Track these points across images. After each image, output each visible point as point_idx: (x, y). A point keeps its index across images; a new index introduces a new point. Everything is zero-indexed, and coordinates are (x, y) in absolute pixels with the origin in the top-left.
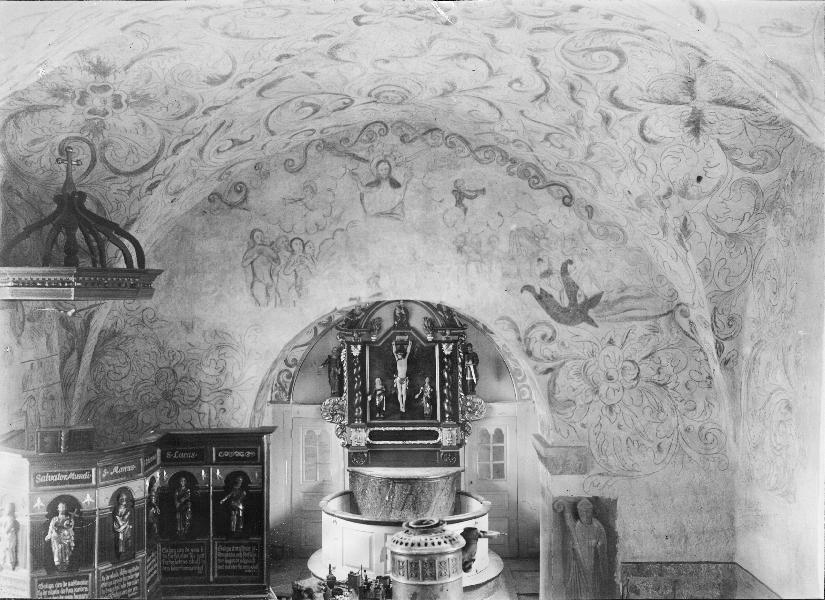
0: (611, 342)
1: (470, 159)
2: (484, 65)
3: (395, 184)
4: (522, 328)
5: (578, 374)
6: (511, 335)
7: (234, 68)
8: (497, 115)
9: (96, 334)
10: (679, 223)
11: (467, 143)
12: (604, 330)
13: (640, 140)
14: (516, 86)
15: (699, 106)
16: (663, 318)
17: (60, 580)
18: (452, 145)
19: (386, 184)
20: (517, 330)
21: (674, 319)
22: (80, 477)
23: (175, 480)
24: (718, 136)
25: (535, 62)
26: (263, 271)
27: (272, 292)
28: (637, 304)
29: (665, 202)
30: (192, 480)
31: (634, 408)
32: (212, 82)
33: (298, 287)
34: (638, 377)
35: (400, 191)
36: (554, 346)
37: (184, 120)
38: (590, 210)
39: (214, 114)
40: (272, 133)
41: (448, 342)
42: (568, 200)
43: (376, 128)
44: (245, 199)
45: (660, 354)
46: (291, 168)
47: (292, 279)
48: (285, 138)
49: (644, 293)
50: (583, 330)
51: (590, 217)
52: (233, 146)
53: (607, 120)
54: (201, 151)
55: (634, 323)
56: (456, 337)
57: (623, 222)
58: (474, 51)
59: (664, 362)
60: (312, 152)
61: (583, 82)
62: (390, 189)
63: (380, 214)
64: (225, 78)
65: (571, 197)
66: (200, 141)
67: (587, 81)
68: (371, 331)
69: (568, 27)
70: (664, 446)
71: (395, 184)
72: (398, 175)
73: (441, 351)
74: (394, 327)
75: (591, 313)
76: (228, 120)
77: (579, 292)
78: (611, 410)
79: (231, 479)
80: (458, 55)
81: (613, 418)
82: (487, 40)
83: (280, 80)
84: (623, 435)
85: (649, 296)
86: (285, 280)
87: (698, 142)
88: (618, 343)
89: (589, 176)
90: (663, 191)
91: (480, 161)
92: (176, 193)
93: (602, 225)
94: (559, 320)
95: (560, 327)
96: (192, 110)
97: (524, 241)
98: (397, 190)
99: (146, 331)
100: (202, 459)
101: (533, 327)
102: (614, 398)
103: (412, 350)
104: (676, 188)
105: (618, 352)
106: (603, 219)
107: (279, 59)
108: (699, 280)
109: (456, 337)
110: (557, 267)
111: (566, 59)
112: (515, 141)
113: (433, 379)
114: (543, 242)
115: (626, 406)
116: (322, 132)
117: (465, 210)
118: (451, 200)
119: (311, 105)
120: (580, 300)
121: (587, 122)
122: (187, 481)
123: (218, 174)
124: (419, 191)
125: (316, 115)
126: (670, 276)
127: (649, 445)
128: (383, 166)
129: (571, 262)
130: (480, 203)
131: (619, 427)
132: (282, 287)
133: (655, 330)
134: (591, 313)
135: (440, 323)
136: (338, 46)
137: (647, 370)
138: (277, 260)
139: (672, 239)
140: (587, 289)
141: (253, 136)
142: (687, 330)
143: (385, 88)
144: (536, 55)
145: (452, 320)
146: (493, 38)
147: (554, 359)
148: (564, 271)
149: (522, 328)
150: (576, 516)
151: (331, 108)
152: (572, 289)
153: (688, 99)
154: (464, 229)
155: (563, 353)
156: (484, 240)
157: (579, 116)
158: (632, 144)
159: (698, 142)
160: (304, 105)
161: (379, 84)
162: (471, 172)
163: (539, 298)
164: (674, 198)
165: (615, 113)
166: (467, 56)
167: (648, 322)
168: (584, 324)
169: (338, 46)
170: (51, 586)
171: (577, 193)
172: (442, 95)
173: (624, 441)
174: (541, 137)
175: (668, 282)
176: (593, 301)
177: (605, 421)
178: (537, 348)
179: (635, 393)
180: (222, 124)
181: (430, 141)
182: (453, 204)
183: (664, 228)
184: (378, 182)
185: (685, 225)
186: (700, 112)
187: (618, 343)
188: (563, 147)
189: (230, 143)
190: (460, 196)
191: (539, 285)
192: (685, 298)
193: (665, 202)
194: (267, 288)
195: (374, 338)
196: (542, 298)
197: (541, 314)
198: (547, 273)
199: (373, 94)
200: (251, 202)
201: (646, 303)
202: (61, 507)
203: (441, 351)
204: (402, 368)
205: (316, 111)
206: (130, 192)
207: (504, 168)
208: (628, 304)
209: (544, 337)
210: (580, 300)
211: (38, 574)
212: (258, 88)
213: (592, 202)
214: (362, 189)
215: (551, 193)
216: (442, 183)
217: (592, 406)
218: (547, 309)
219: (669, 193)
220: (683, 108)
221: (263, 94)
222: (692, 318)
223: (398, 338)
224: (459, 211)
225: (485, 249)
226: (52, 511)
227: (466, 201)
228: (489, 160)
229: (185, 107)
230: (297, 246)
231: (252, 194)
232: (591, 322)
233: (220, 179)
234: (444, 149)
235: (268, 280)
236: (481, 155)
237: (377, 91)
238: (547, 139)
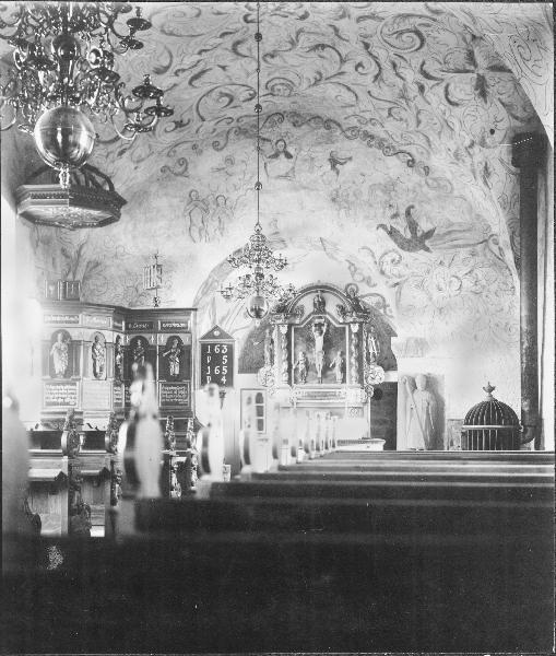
1: (342, 137)
3: (289, 156)
4: (378, 255)
6: (369, 260)
7: (171, 61)
8: (354, 99)
9: (85, 264)
10: (482, 167)
11: (339, 125)
12: (434, 255)
13: (446, 103)
15: (481, 72)
16: (480, 246)
17: (59, 384)
18: (328, 128)
19: (282, 156)
20: (373, 256)
21: (487, 246)
22: (72, 319)
23: (134, 342)
24: (498, 96)
25: (367, 46)
26: (197, 218)
27: (203, 233)
28: (459, 235)
29: (470, 150)
30: (145, 341)
33: (222, 229)
36: (400, 267)
38: (427, 170)
41: (354, 323)
42: (411, 163)
43: (276, 118)
44: (186, 169)
45: (475, 271)
46: (216, 146)
47: (217, 223)
49: (465, 228)
50: (421, 255)
51: (427, 173)
52: (176, 127)
53: (422, 89)
55: (458, 249)
56: (362, 320)
57: (449, 176)
58: (327, 42)
59: (480, 276)
60: (232, 136)
61: (402, 61)
62: (286, 160)
63: (279, 177)
64: (167, 68)
65: (413, 161)
67: (402, 57)
68: (295, 315)
69: (381, 15)
70: (361, 179)
71: (289, 156)
72: (291, 150)
73: (350, 330)
74: (313, 313)
75: (427, 243)
79: (170, 340)
80: (317, 47)
82: (331, 30)
83: (203, 72)
85: (469, 230)
86: (212, 226)
87: (486, 102)
88: (446, 263)
89: (421, 141)
90: (467, 143)
91: (348, 137)
92: (138, 162)
93: (435, 180)
94: (403, 248)
95: (405, 254)
97: (379, 193)
99: (118, 261)
100: (152, 328)
101: (386, 254)
103: (327, 330)
104: (477, 140)
105: (447, 271)
106: (436, 175)
107: (200, 53)
108: (500, 210)
109: (362, 320)
110: (403, 211)
111: (385, 41)
112: (371, 119)
113: (343, 354)
114: (393, 193)
116: (238, 120)
117: (338, 173)
118: (328, 167)
119: (227, 95)
120: (419, 234)
121: (411, 95)
122: (142, 343)
123: (166, 151)
124: (306, 160)
125: (232, 105)
126: (485, 215)
128: (281, 143)
129: (413, 207)
130: (349, 166)
132: (211, 229)
133: (473, 254)
134: (427, 243)
135: (349, 308)
136: (238, 43)
138: (206, 211)
139: (480, 181)
140: (424, 226)
142: (497, 253)
143: (277, 81)
144: (366, 41)
145: (358, 305)
146: (336, 30)
147: (400, 276)
148: (408, 213)
149: (378, 255)
150: (415, 387)
151: (242, 99)
152: (413, 226)
153: (472, 68)
155: (407, 272)
156: (351, 194)
157: (405, 89)
158: (442, 107)
159: (486, 102)
160: (223, 95)
161: (272, 77)
162: (344, 147)
163: (390, 233)
164: (477, 148)
165: (428, 83)
166: (323, 46)
167: (468, 249)
168: (422, 251)
169: (238, 43)
170: (53, 387)
171: (418, 158)
172: (315, 84)
174: (386, 114)
175: (484, 220)
176: (428, 235)
178: (387, 268)
181: (313, 125)
182: (329, 167)
183: (473, 172)
184: (276, 156)
185: (486, 168)
186: (483, 77)
187: (446, 263)
188: (401, 119)
189: (174, 125)
190: (334, 162)
191: (389, 223)
192: (495, 230)
193: (470, 150)
194: (200, 230)
195: (297, 321)
196: (392, 233)
197: (392, 244)
198: (395, 216)
200: (191, 171)
201: (467, 235)
202: (60, 336)
203: (350, 330)
204: (319, 341)
205: (231, 101)
206: (107, 156)
207: (365, 143)
208: (453, 236)
209: (393, 261)
210: (419, 234)
213: (427, 163)
214: (266, 160)
215: (399, 158)
216: (322, 154)
218: (395, 241)
219: (472, 144)
220: (470, 75)
222: (501, 245)
223: (317, 321)
224: (334, 173)
225: (351, 198)
226: (54, 339)
227: (338, 166)
228: (355, 137)
230: (221, 200)
231: (190, 166)
232: (427, 250)
234: (323, 131)
235: (201, 225)
236: (349, 134)
238: (390, 114)
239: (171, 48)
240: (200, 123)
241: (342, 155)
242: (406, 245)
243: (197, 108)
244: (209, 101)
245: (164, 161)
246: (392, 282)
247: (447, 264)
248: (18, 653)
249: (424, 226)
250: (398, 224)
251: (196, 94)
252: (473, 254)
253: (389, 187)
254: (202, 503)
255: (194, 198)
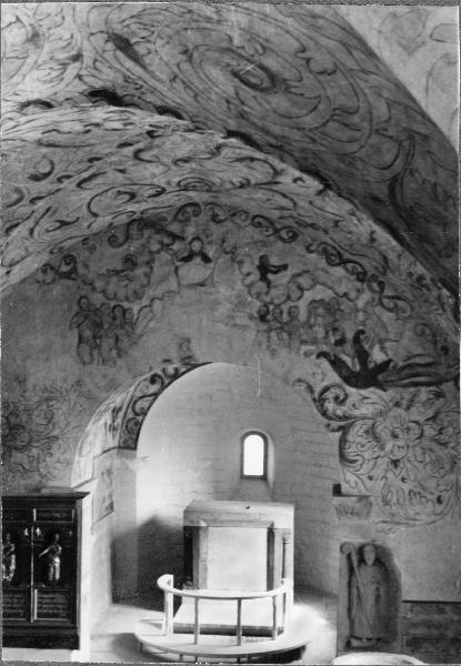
0: (397, 404)
2: (268, 166)
3: (206, 259)
4: (318, 390)
5: (367, 432)
14: (299, 183)
28: (420, 370)
31: (416, 464)
32: (36, 178)
34: (421, 435)
35: (212, 265)
37: (14, 208)
39: (40, 204)
40: (95, 215)
45: (442, 416)
48: (109, 219)
50: (372, 393)
54: (31, 231)
55: (419, 388)
65: (365, 273)
66: (30, 223)
71: (206, 259)
72: (211, 252)
76: (55, 206)
77: (370, 359)
78: (396, 466)
81: (397, 472)
84: (406, 487)
92: (11, 266)
95: (351, 390)
96: (19, 200)
98: (208, 265)
102: (398, 454)
110: (350, 335)
115: (409, 461)
118: (256, 276)
122: (11, 536)
127: (430, 497)
129: (362, 332)
131: (403, 480)
137: (429, 431)
140: (378, 356)
141: (78, 219)
148: (356, 340)
150: (362, 560)
152: (363, 356)
154: (268, 299)
173: (407, 492)
176: (383, 367)
177: (390, 475)
178: (330, 406)
179: (418, 451)
180: (48, 210)
187: (405, 403)
196: (337, 364)
198: (340, 342)
199: (182, 184)
209: (336, 398)
211: (72, 632)
212: (77, 181)
217: (379, 461)
221: (83, 186)
229: (15, 196)
233: (51, 252)
237: (185, 182)
239: (52, 157)
240: (93, 219)
241: (274, 261)
242: (351, 379)
243: (89, 204)
244: (105, 200)
245: (45, 257)
246: (335, 424)
247: (404, 406)
248: (439, 662)
249: (378, 356)
250: (344, 352)
251: (86, 195)
252: (439, 395)
253: (331, 308)
254: (156, 584)
255: (85, 308)
